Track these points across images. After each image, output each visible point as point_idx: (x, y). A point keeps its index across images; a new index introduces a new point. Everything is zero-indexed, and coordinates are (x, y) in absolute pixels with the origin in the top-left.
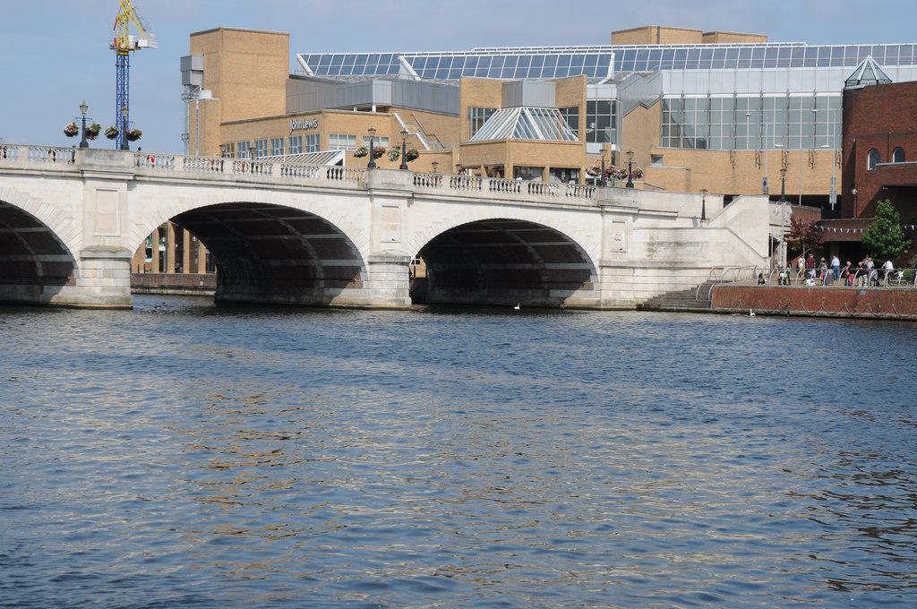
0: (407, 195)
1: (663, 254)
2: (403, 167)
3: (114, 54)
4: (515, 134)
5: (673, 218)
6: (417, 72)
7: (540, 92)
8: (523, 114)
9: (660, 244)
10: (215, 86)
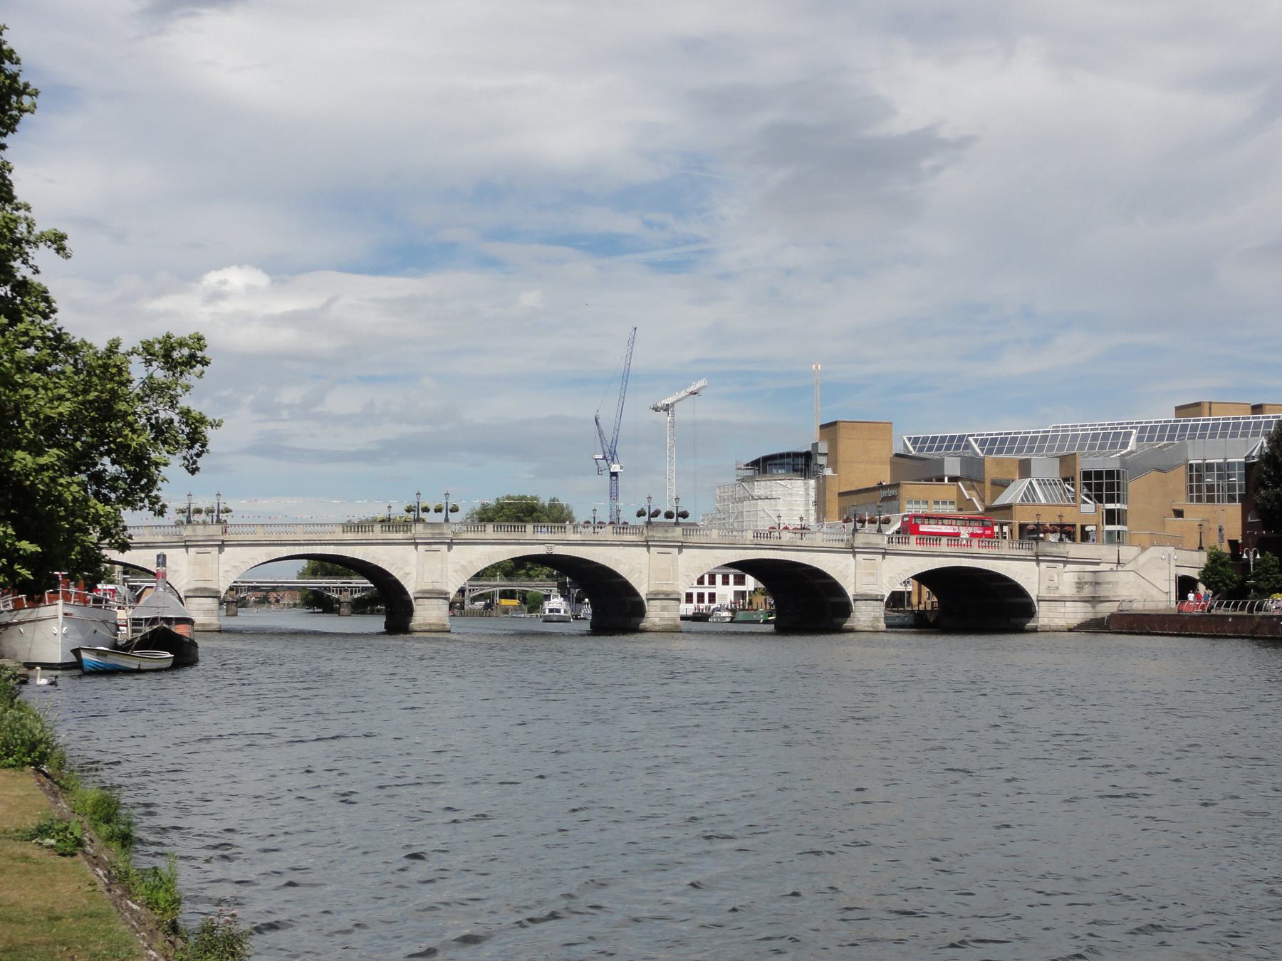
0: (881, 551)
1: (1087, 591)
2: (879, 531)
4: (1022, 499)
5: (1098, 564)
6: (980, 449)
8: (1031, 483)
9: (1086, 583)
10: (833, 464)
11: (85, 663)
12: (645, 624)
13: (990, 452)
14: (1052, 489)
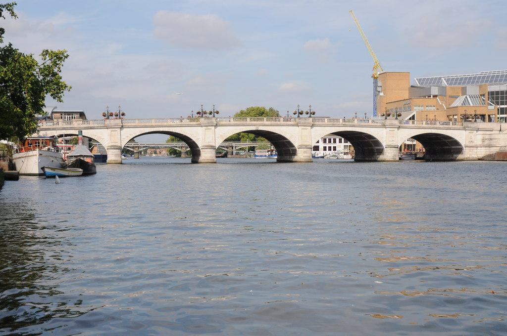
1: (487, 142)
2: (396, 119)
3: (373, 79)
4: (462, 104)
7: (473, 90)
8: (466, 97)
9: (486, 139)
10: (384, 91)
11: (46, 173)
12: (296, 158)
13: (451, 84)
14: (473, 99)
